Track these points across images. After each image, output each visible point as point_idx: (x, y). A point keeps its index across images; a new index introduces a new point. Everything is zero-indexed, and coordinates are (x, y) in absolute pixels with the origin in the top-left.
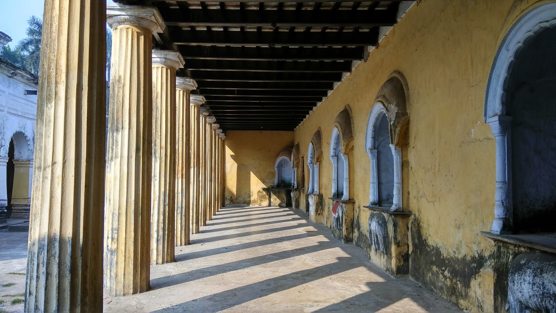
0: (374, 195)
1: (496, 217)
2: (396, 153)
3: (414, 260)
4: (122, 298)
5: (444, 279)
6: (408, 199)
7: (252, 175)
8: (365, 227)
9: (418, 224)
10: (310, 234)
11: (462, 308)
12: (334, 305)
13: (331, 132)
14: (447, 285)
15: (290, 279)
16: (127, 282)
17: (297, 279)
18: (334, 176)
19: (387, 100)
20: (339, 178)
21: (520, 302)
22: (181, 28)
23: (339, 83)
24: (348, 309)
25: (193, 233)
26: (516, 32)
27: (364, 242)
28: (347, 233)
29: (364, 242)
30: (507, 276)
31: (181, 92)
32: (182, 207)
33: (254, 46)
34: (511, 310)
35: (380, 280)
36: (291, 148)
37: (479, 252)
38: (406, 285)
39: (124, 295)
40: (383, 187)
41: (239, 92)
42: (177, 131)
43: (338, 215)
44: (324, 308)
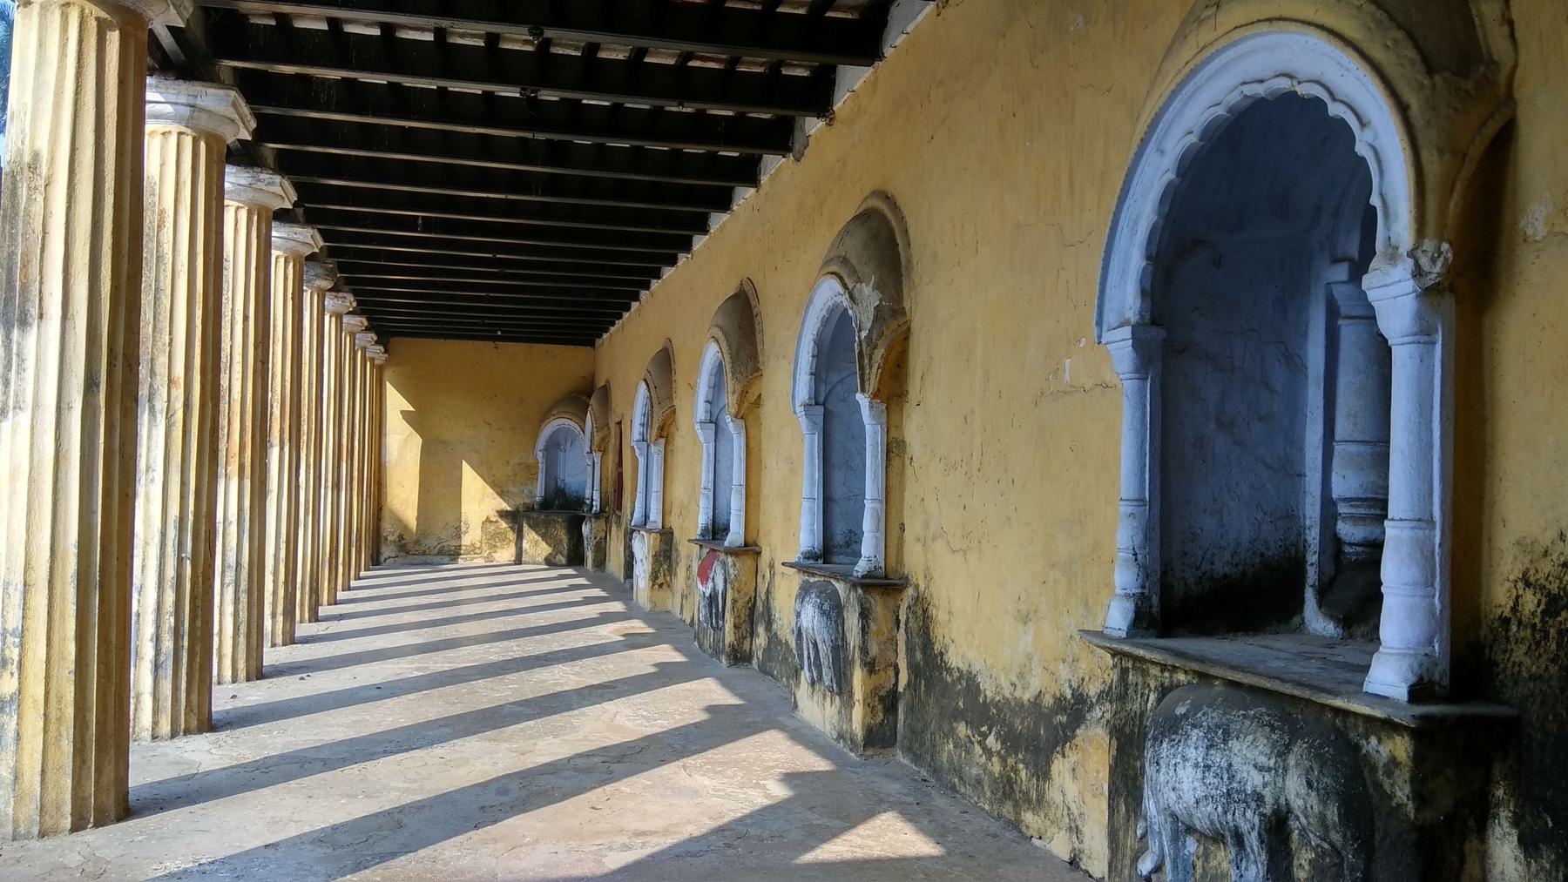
0: (812, 531)
1: (1118, 591)
2: (873, 417)
3: (911, 709)
4: (36, 844)
5: (984, 757)
6: (901, 541)
7: (467, 471)
8: (786, 622)
9: (925, 611)
10: (633, 642)
11: (1029, 834)
12: (692, 840)
13: (700, 354)
14: (991, 774)
15: (567, 774)
16: (51, 794)
17: (588, 771)
18: (705, 477)
19: (853, 272)
20: (721, 485)
21: (1174, 815)
22: (245, 17)
23: (725, 217)
24: (730, 852)
25: (274, 645)
26: (1185, 104)
27: (782, 663)
28: (737, 640)
29: (782, 663)
30: (1142, 749)
31: (243, 214)
32: (238, 564)
33: (476, 89)
34: (1149, 836)
35: (822, 765)
36: (586, 396)
37: (1075, 685)
38: (886, 776)
39: (42, 835)
40: (836, 510)
41: (429, 225)
42: (226, 332)
43: (714, 588)
44: (662, 852)
